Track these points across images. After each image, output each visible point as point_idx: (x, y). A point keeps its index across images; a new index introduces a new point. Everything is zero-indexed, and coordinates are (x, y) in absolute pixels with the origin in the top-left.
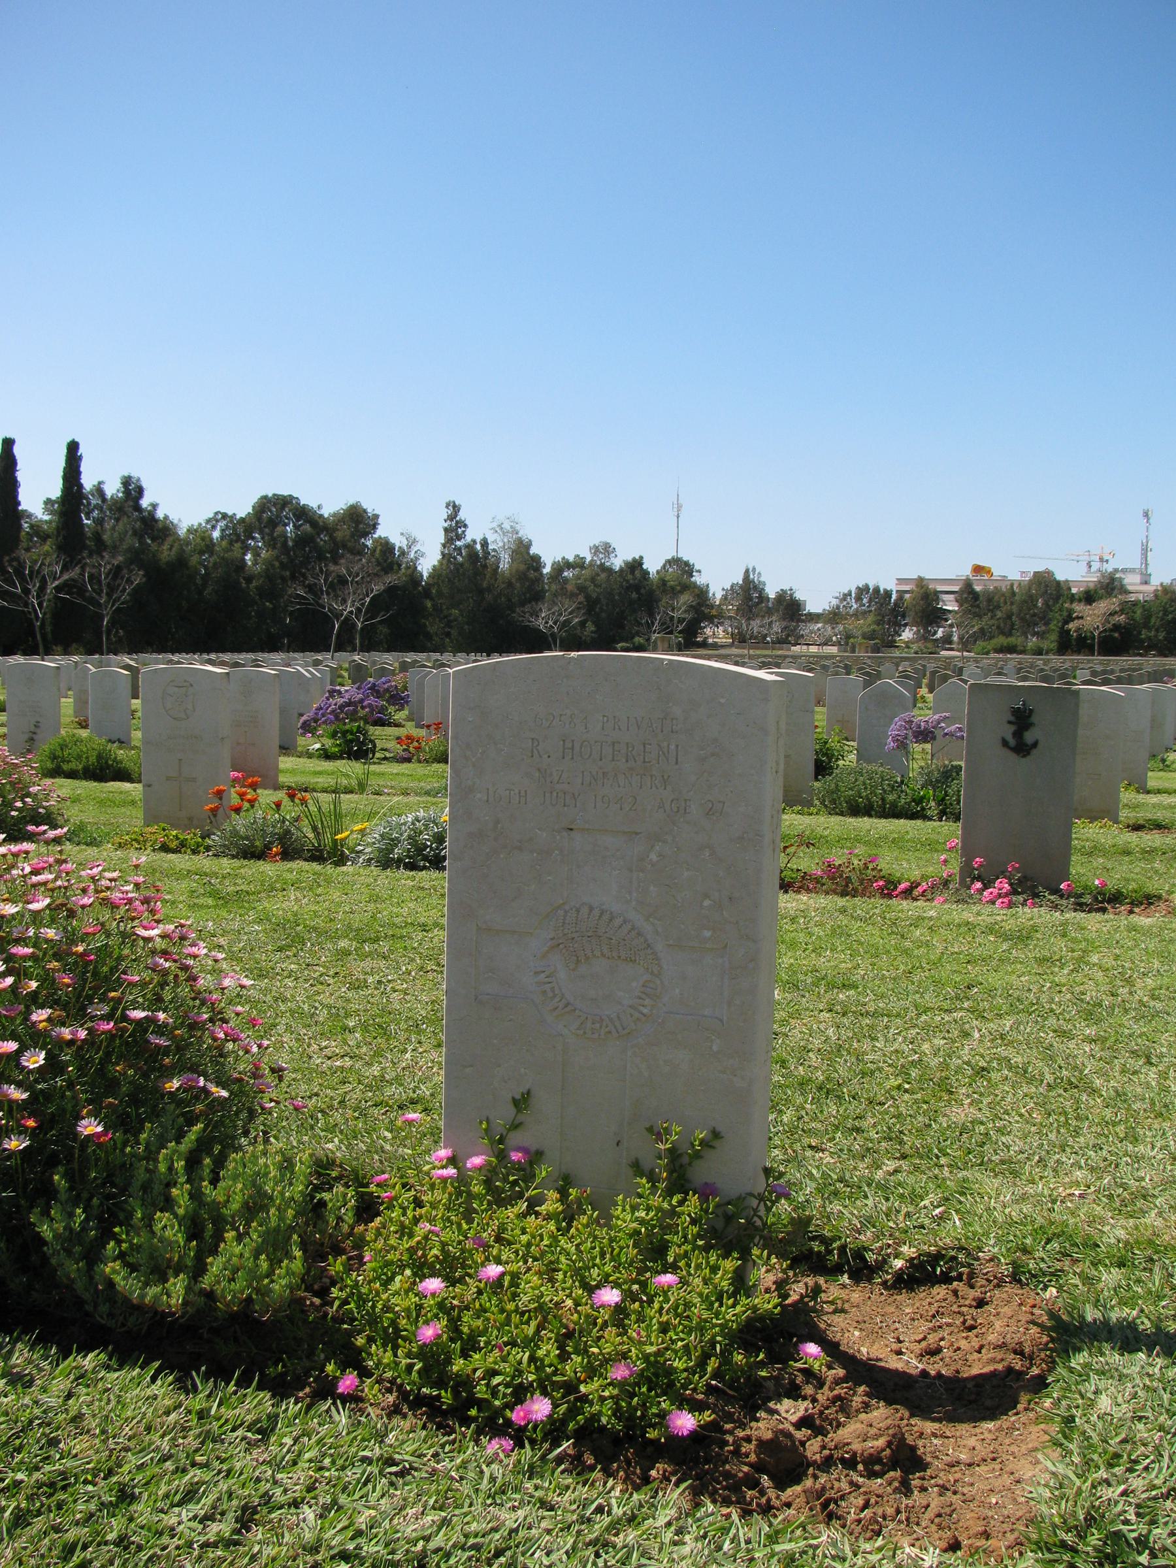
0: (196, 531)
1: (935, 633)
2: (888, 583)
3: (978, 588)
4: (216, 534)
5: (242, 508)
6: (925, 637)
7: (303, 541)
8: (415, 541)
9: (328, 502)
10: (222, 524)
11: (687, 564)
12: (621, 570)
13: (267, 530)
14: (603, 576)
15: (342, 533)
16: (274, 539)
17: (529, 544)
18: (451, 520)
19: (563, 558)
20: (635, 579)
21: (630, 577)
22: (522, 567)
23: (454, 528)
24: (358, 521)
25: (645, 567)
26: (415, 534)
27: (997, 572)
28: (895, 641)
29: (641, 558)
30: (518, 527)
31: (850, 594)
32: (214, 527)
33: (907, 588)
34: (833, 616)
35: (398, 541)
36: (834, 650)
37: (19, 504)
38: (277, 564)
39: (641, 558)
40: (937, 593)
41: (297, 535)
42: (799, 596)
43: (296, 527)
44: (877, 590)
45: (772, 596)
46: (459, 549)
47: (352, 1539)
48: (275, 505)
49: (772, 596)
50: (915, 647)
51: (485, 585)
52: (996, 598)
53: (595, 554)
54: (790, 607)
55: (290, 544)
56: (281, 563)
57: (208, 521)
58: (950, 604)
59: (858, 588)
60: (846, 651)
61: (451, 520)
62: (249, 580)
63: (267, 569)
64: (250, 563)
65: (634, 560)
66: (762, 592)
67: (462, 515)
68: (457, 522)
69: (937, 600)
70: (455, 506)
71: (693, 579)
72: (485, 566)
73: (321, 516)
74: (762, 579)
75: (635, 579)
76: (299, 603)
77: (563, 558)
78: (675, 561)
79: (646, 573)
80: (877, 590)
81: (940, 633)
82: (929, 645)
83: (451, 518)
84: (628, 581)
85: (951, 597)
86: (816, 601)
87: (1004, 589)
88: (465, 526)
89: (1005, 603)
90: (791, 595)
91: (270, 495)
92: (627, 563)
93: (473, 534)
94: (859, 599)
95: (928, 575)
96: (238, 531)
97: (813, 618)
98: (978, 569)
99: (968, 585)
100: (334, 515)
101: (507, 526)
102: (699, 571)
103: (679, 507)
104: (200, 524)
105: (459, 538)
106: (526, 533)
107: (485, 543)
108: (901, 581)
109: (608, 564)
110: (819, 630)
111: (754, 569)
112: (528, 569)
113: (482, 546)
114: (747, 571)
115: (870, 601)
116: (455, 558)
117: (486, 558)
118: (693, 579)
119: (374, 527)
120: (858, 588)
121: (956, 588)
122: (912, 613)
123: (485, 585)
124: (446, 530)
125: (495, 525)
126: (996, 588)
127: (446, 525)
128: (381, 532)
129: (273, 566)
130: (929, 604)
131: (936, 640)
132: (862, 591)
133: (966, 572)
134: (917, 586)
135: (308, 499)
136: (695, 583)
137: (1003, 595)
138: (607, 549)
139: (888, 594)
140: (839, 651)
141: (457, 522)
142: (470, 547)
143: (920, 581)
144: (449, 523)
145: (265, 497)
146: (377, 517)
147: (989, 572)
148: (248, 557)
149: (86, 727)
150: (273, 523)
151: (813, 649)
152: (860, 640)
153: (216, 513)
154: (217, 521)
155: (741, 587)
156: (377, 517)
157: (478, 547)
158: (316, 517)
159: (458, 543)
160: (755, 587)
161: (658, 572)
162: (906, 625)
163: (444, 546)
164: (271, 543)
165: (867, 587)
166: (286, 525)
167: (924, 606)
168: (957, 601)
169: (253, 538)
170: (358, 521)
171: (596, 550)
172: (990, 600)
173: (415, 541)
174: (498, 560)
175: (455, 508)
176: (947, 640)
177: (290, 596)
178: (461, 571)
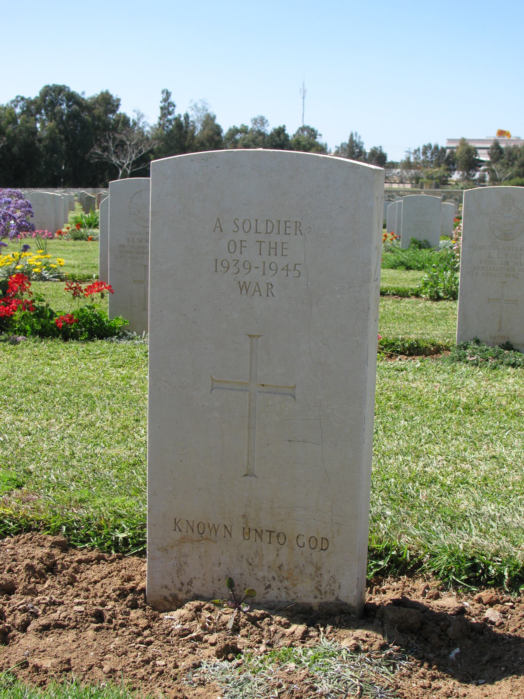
0: (5, 108)
1: (474, 175)
2: (443, 144)
3: (503, 146)
4: (18, 110)
5: (33, 93)
6: (467, 178)
7: (73, 116)
8: (142, 116)
9: (88, 89)
10: (21, 104)
11: (313, 130)
12: (272, 134)
13: (49, 109)
14: (261, 138)
15: (98, 111)
16: (54, 114)
17: (214, 118)
18: (165, 102)
19: (234, 127)
20: (280, 140)
21: (277, 139)
22: (211, 133)
23: (167, 108)
24: (107, 102)
25: (286, 132)
26: (143, 111)
27: (514, 134)
28: (448, 181)
29: (284, 126)
30: (207, 107)
31: (419, 150)
32: (16, 106)
33: (454, 145)
34: (408, 165)
35: (132, 116)
36: (408, 186)
37: (37, 97)
38: (57, 131)
39: (284, 126)
40: (475, 149)
41: (68, 112)
42: (384, 151)
43: (68, 106)
44: (436, 147)
45: (368, 151)
46: (170, 121)
47: (333, 643)
48: (54, 91)
49: (368, 151)
50: (461, 185)
51: (187, 144)
52: (515, 152)
53: (255, 124)
54: (378, 157)
55: (64, 118)
56: (60, 130)
57: (12, 102)
58: (484, 156)
59: (425, 146)
60: (416, 187)
61: (165, 102)
62: (40, 141)
63: (51, 134)
64: (39, 130)
65: (280, 128)
66: (361, 148)
67: (172, 99)
68: (169, 104)
69: (476, 154)
70: (167, 93)
71: (317, 140)
72: (186, 132)
73: (83, 99)
74: (361, 140)
75: (280, 140)
76: (98, 158)
77: (234, 127)
78: (303, 129)
79: (287, 136)
80: (436, 147)
81: (477, 175)
82: (471, 183)
83: (166, 100)
84: (276, 141)
85: (485, 151)
86: (395, 156)
87: (520, 146)
88: (174, 106)
89: (521, 156)
90: (381, 151)
91: (51, 85)
92: (275, 130)
93: (180, 111)
94: (424, 153)
95: (468, 137)
96: (32, 108)
97: (394, 165)
98: (501, 133)
99: (496, 145)
100: (91, 98)
101: (200, 106)
102: (320, 135)
103: (305, 92)
104: (8, 104)
105: (170, 113)
106: (212, 110)
107: (187, 117)
108: (450, 141)
109: (262, 131)
110: (398, 173)
111: (356, 134)
112: (214, 134)
113: (185, 118)
114: (352, 135)
115: (432, 154)
116: (167, 127)
117: (187, 127)
118: (317, 140)
119: (118, 106)
120: (425, 146)
121: (489, 145)
122: (460, 162)
123: (187, 144)
124: (162, 108)
125: (192, 105)
126: (514, 146)
127: (162, 105)
128: (121, 110)
129: (54, 132)
130: (471, 157)
131: (475, 180)
132: (427, 148)
133: (493, 135)
134: (461, 144)
135: (76, 88)
136: (318, 143)
137: (519, 150)
138: (262, 121)
139: (444, 150)
140: (412, 187)
141: (169, 104)
142: (177, 119)
143: (463, 142)
144: (163, 103)
145: (48, 87)
146: (119, 100)
147: (508, 134)
148: (38, 125)
149: (96, 226)
150: (53, 104)
151: (395, 186)
152: (425, 180)
153: (17, 97)
154: (18, 102)
155: (348, 145)
156: (119, 100)
157: (182, 119)
158: (80, 100)
159: (170, 117)
160: (357, 146)
161: (294, 136)
162: (455, 170)
163: (160, 119)
164: (53, 116)
165: (430, 146)
166: (61, 105)
167: (464, 158)
168: (489, 154)
169: (40, 113)
170: (107, 102)
171: (255, 121)
172: (510, 154)
173: (142, 116)
174: (195, 128)
175: (168, 94)
176: (482, 180)
177: (92, 153)
178: (171, 135)
